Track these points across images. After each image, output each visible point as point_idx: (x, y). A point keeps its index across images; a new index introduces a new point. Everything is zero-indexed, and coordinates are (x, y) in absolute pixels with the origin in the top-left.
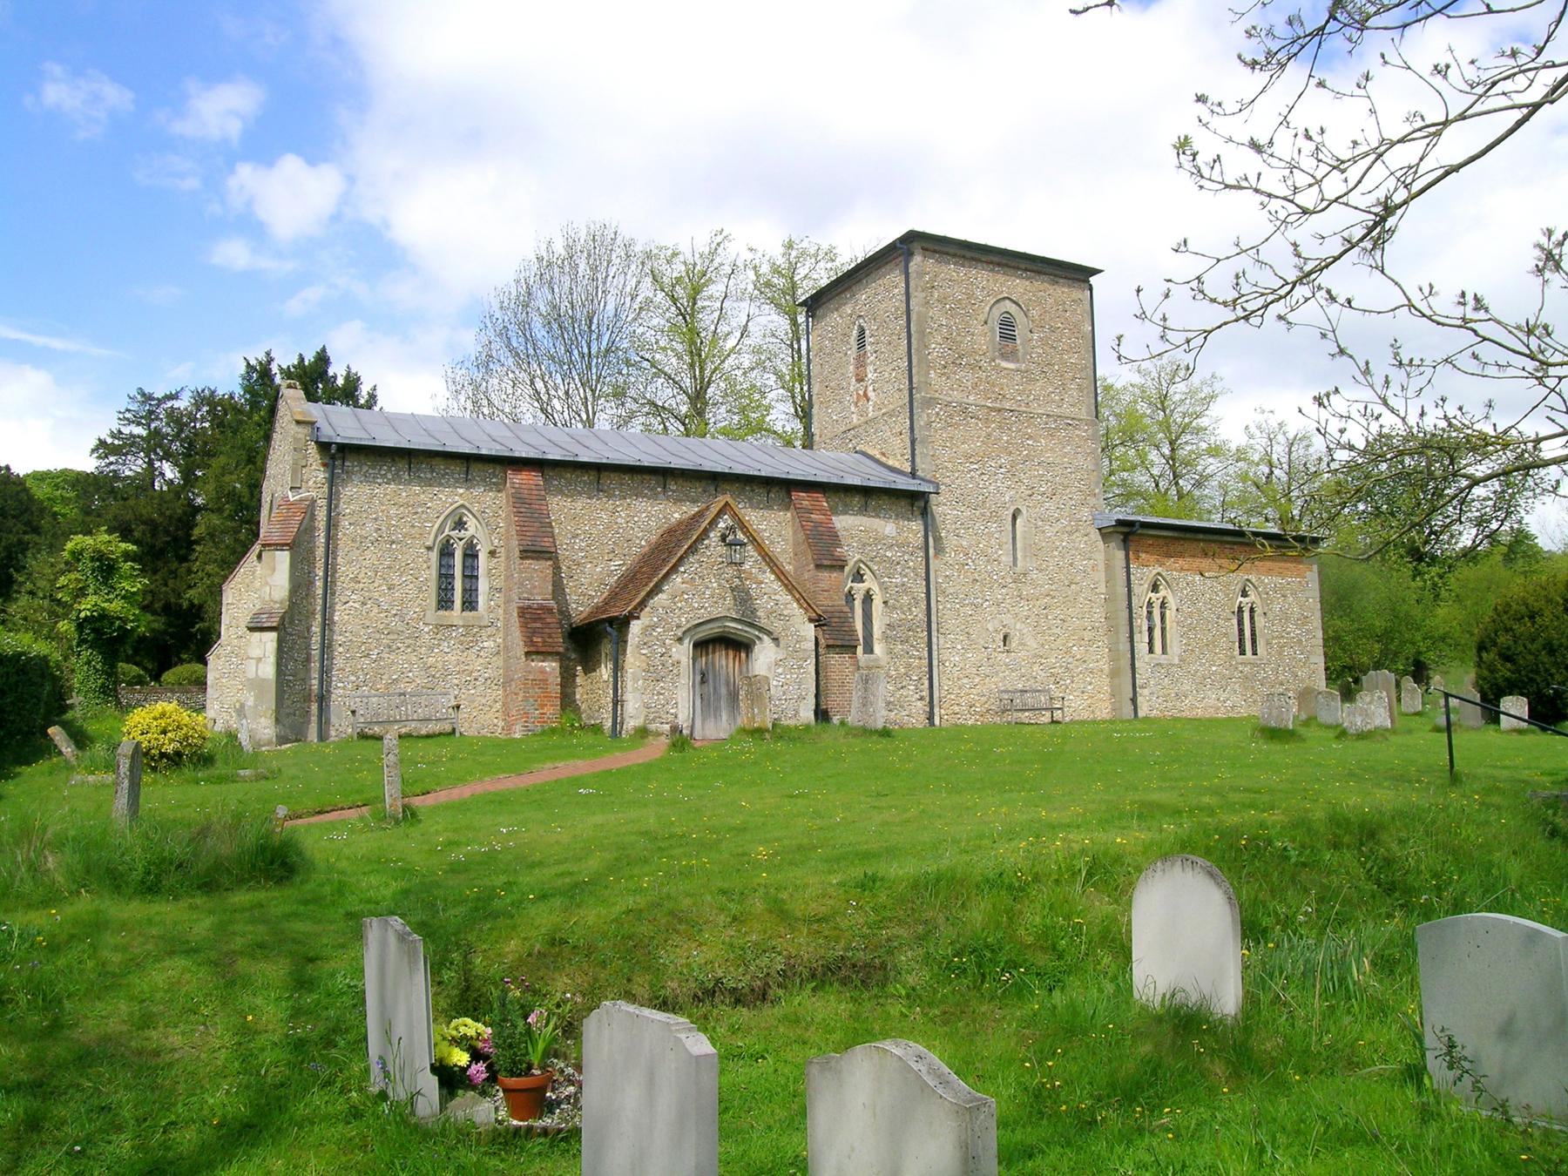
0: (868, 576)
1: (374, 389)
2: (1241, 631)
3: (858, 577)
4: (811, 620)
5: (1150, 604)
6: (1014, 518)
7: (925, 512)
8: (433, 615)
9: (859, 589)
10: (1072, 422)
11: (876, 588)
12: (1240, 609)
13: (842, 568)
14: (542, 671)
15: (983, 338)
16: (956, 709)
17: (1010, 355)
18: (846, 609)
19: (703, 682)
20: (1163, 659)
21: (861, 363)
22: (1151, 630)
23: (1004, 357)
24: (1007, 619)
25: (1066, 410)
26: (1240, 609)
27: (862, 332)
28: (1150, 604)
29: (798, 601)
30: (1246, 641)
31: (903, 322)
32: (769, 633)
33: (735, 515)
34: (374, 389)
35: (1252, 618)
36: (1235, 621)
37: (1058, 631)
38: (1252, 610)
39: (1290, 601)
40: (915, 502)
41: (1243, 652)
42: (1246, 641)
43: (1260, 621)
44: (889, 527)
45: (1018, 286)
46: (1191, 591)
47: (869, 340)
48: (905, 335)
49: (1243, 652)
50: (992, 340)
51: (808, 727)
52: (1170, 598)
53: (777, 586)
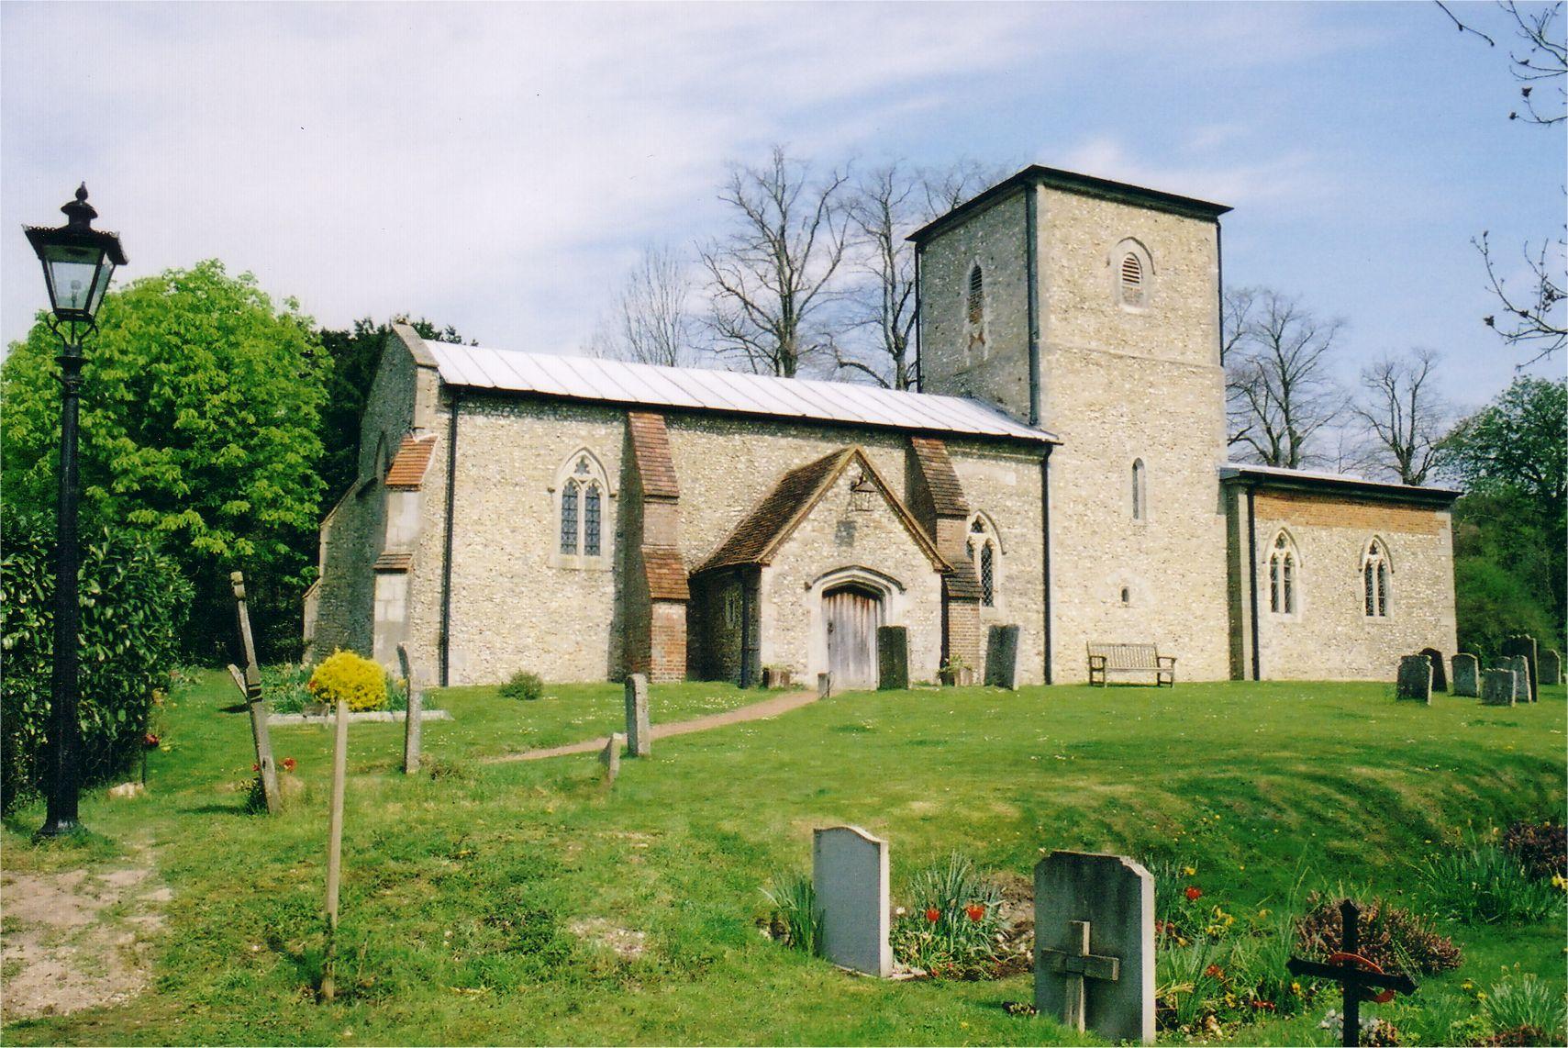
0: (987, 526)
1: (82, 193)
2: (1369, 590)
3: (978, 527)
4: (937, 570)
5: (1274, 560)
6: (1135, 467)
7: (1044, 465)
8: (557, 556)
9: (979, 540)
10: (1196, 371)
11: (995, 540)
12: (1369, 568)
13: (964, 517)
14: (668, 618)
15: (1106, 280)
16: (1074, 665)
17: (1134, 299)
18: (968, 560)
19: (830, 631)
20: (1287, 618)
21: (976, 305)
22: (1274, 587)
23: (1127, 300)
24: (1126, 573)
25: (1190, 357)
26: (1369, 568)
27: (977, 273)
28: (1274, 560)
29: (924, 551)
30: (1375, 601)
31: (1023, 262)
32: (898, 584)
33: (864, 464)
34: (82, 193)
35: (1380, 576)
36: (1362, 580)
37: (1177, 586)
38: (1381, 568)
39: (1424, 556)
40: (1039, 451)
41: (1370, 613)
42: (1375, 601)
43: (1390, 581)
44: (1013, 475)
45: (1143, 221)
46: (1319, 546)
47: (985, 280)
48: (1025, 277)
49: (1370, 613)
50: (1116, 282)
51: (869, 693)
52: (1294, 555)
53: (905, 536)
